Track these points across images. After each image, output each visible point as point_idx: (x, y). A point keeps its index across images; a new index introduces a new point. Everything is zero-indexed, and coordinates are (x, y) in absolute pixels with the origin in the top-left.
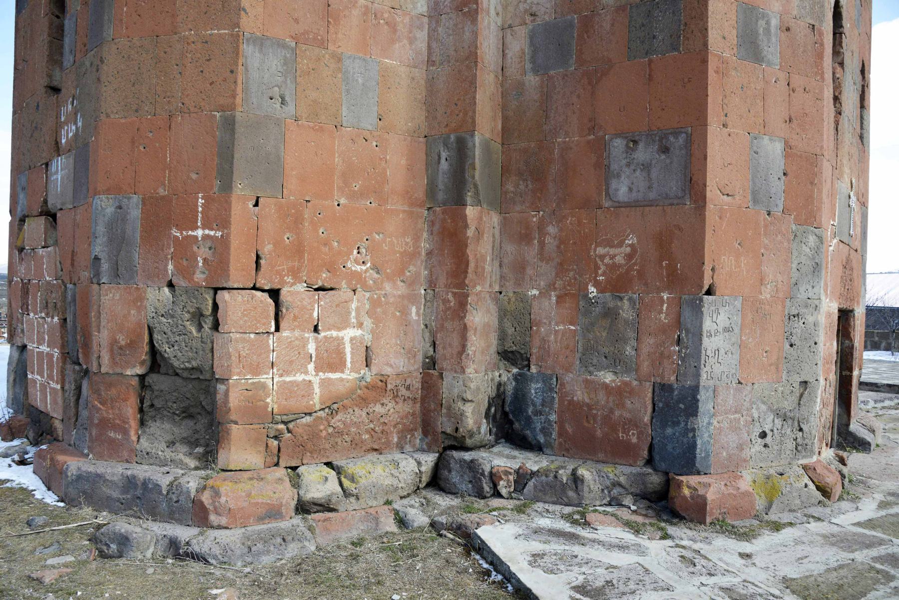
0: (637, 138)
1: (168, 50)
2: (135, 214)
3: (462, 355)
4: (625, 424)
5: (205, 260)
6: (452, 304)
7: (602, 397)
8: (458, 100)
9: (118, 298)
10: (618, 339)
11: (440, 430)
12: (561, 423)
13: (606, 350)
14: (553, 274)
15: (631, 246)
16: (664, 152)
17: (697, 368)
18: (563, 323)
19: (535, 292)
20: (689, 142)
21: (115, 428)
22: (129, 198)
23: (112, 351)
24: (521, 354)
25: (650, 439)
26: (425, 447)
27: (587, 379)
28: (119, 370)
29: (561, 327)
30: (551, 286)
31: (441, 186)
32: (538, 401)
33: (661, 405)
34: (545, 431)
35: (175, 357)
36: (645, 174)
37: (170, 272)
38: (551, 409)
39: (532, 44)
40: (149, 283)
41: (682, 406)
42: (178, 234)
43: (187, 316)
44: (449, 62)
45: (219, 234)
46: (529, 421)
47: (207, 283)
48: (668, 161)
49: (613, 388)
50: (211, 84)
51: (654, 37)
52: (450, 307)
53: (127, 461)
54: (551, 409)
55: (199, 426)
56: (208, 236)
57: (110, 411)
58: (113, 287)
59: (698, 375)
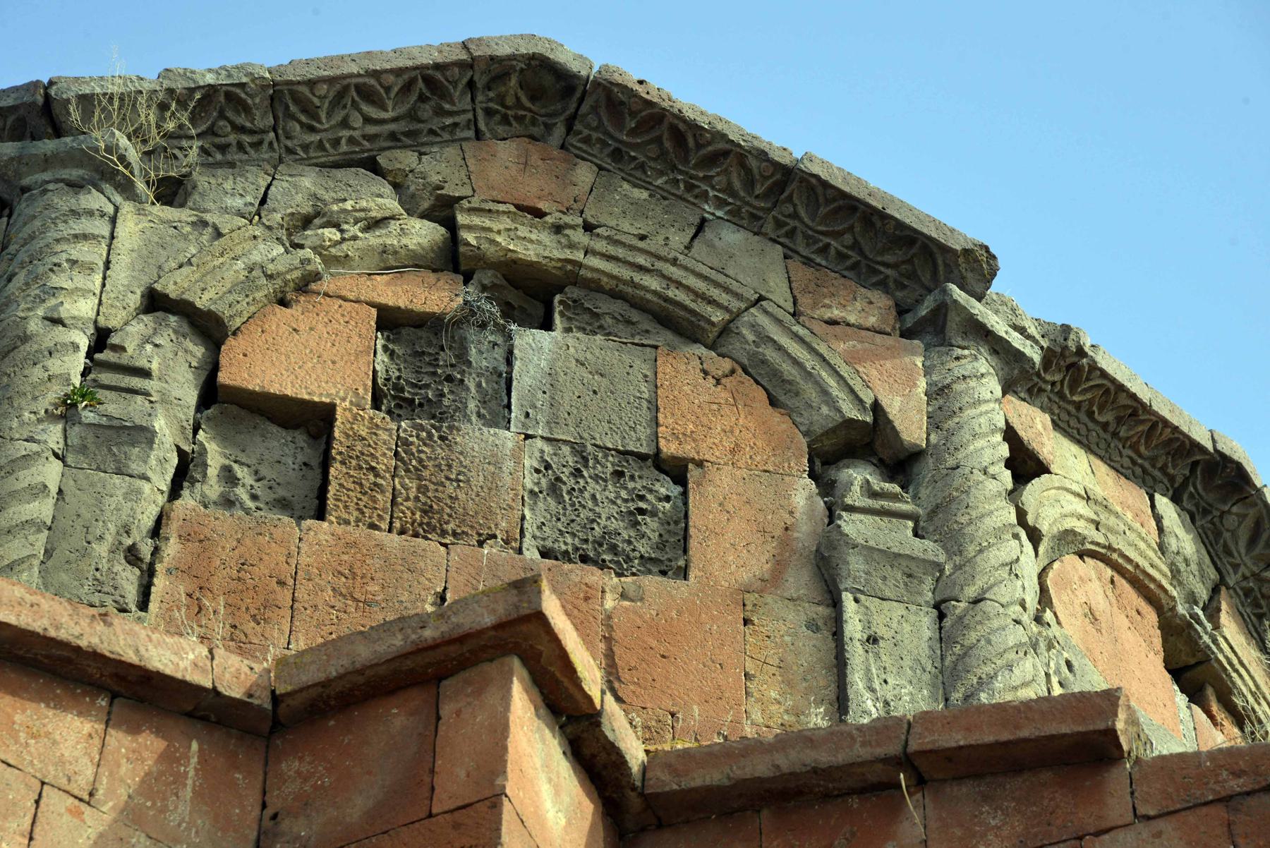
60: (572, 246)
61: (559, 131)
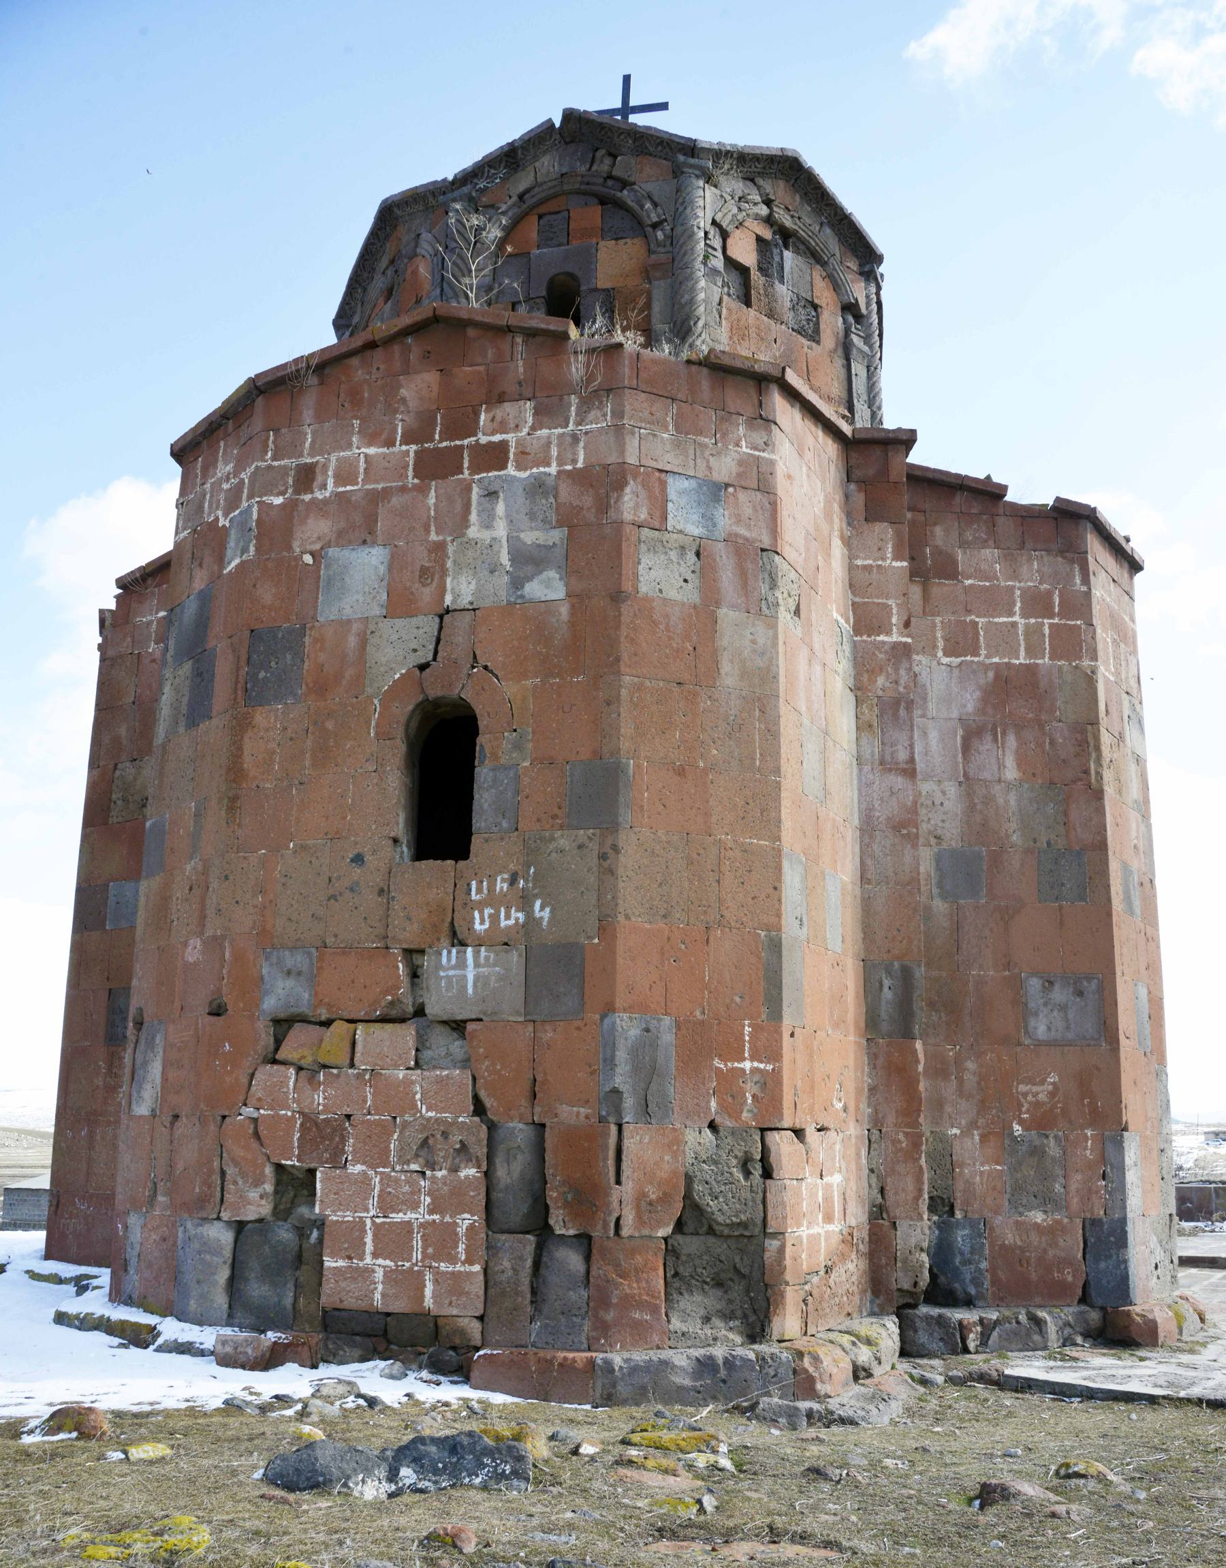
0: (1052, 979)
1: (702, 851)
2: (668, 1037)
3: (918, 1200)
4: (1060, 1263)
5: (753, 1096)
6: (904, 1145)
7: (1034, 1238)
8: (901, 925)
9: (646, 1141)
10: (1046, 1177)
11: (894, 1287)
12: (993, 1269)
13: (1035, 1189)
14: (975, 1112)
15: (1054, 1084)
16: (1078, 995)
17: (1124, 1201)
18: (988, 1162)
19: (955, 1131)
20: (1101, 989)
21: (641, 1305)
22: (659, 1020)
23: (638, 1207)
24: (942, 1199)
25: (1084, 1275)
26: (876, 1309)
27: (1017, 1221)
28: (646, 1232)
29: (987, 1168)
30: (973, 1125)
31: (884, 1015)
32: (967, 1249)
33: (1093, 1240)
34: (976, 1282)
35: (720, 1210)
36: (1062, 1014)
37: (713, 1110)
38: (981, 1256)
39: (938, 868)
40: (688, 1123)
41: (1112, 1239)
42: (722, 1066)
43: (734, 1162)
44: (888, 883)
45: (769, 1067)
46: (957, 1273)
47: (757, 1122)
48: (1083, 1003)
49: (1044, 1227)
50: (753, 898)
51: (1063, 884)
52: (901, 1149)
53: (658, 1348)
54: (981, 1256)
55: (733, 1295)
56: (757, 1069)
57: (635, 1285)
58: (641, 1128)
59: (1124, 1208)
60: (796, 224)
61: (793, 181)
